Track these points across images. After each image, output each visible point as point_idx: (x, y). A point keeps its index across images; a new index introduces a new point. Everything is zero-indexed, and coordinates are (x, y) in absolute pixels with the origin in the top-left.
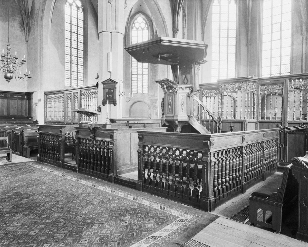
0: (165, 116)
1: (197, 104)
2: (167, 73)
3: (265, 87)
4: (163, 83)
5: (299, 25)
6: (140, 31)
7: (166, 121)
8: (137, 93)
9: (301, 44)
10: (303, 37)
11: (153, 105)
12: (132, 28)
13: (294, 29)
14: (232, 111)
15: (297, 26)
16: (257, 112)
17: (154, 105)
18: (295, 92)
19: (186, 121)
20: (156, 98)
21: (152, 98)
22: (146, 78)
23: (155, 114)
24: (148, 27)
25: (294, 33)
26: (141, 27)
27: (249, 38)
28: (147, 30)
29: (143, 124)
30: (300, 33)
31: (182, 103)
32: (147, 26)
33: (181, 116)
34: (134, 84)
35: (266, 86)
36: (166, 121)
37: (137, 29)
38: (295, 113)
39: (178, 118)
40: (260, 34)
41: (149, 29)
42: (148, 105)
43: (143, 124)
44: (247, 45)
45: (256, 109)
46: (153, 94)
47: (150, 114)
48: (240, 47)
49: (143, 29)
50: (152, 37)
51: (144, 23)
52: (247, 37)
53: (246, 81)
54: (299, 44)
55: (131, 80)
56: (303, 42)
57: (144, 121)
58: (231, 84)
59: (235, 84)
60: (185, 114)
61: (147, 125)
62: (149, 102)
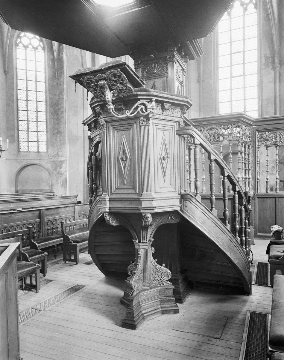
0: (107, 198)
1: (205, 156)
2: (82, 109)
3: (265, 135)
4: (102, 82)
5: (269, 55)
6: (30, 53)
7: (110, 214)
8: (29, 150)
9: (274, 82)
10: (275, 73)
11: (56, 170)
12: (17, 45)
13: (263, 61)
14: (277, 179)
15: (267, 57)
16: (253, 178)
17: (58, 170)
18: (268, 149)
19: (176, 212)
20: (60, 159)
21: (54, 159)
22: (43, 127)
23: (59, 184)
24: (44, 45)
25: (263, 67)
26: (22, 43)
27: (201, 71)
28: (43, 51)
29: (38, 212)
30: (271, 67)
31: (164, 154)
32: (42, 45)
33: (163, 195)
34: (23, 136)
35: (267, 133)
36: (110, 214)
37: (26, 47)
38: (268, 180)
39: (155, 204)
40: (216, 67)
41: (46, 49)
42: (47, 170)
43: (38, 212)
44: (199, 82)
45: (251, 173)
46: (55, 153)
47: (52, 185)
48: (189, 84)
49: (35, 49)
50: (51, 63)
51: (37, 39)
52: (199, 69)
53: (238, 122)
54: (270, 82)
55: (16, 131)
56: (275, 79)
57: (39, 202)
58: (208, 128)
59: (217, 128)
60: (174, 190)
61: (46, 213)
62: (49, 166)
